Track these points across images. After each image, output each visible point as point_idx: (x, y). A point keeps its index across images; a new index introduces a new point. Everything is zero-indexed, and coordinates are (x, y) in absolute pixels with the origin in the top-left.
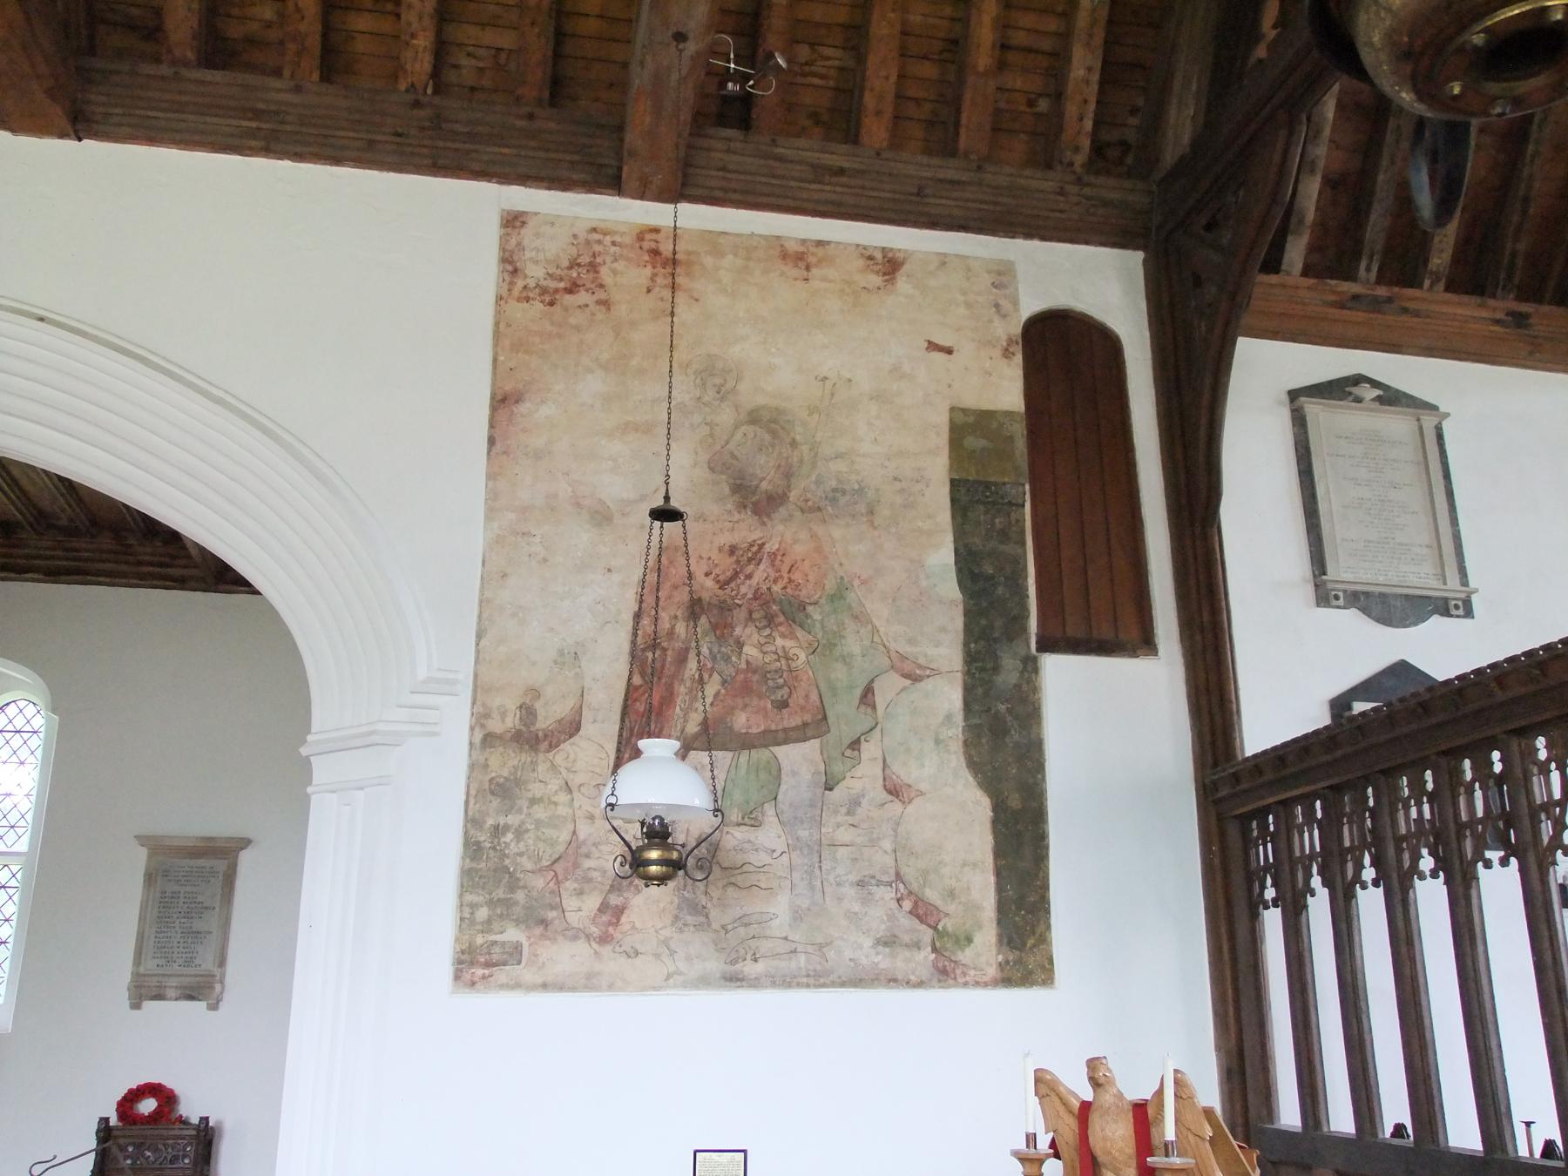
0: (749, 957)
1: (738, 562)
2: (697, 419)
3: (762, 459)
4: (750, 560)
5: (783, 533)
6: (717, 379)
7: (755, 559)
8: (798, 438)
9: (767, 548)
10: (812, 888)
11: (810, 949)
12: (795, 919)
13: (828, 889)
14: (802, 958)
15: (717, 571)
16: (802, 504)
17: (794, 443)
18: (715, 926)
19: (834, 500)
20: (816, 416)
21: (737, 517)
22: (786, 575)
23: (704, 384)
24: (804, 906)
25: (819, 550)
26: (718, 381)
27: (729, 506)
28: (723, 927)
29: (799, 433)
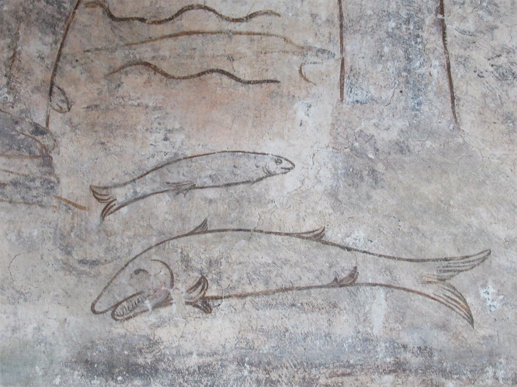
0: (180, 292)
10: (411, 82)
11: (407, 276)
12: (353, 176)
13: (469, 89)
14: (378, 307)
18: (70, 187)
24: (385, 137)
28: (97, 193)
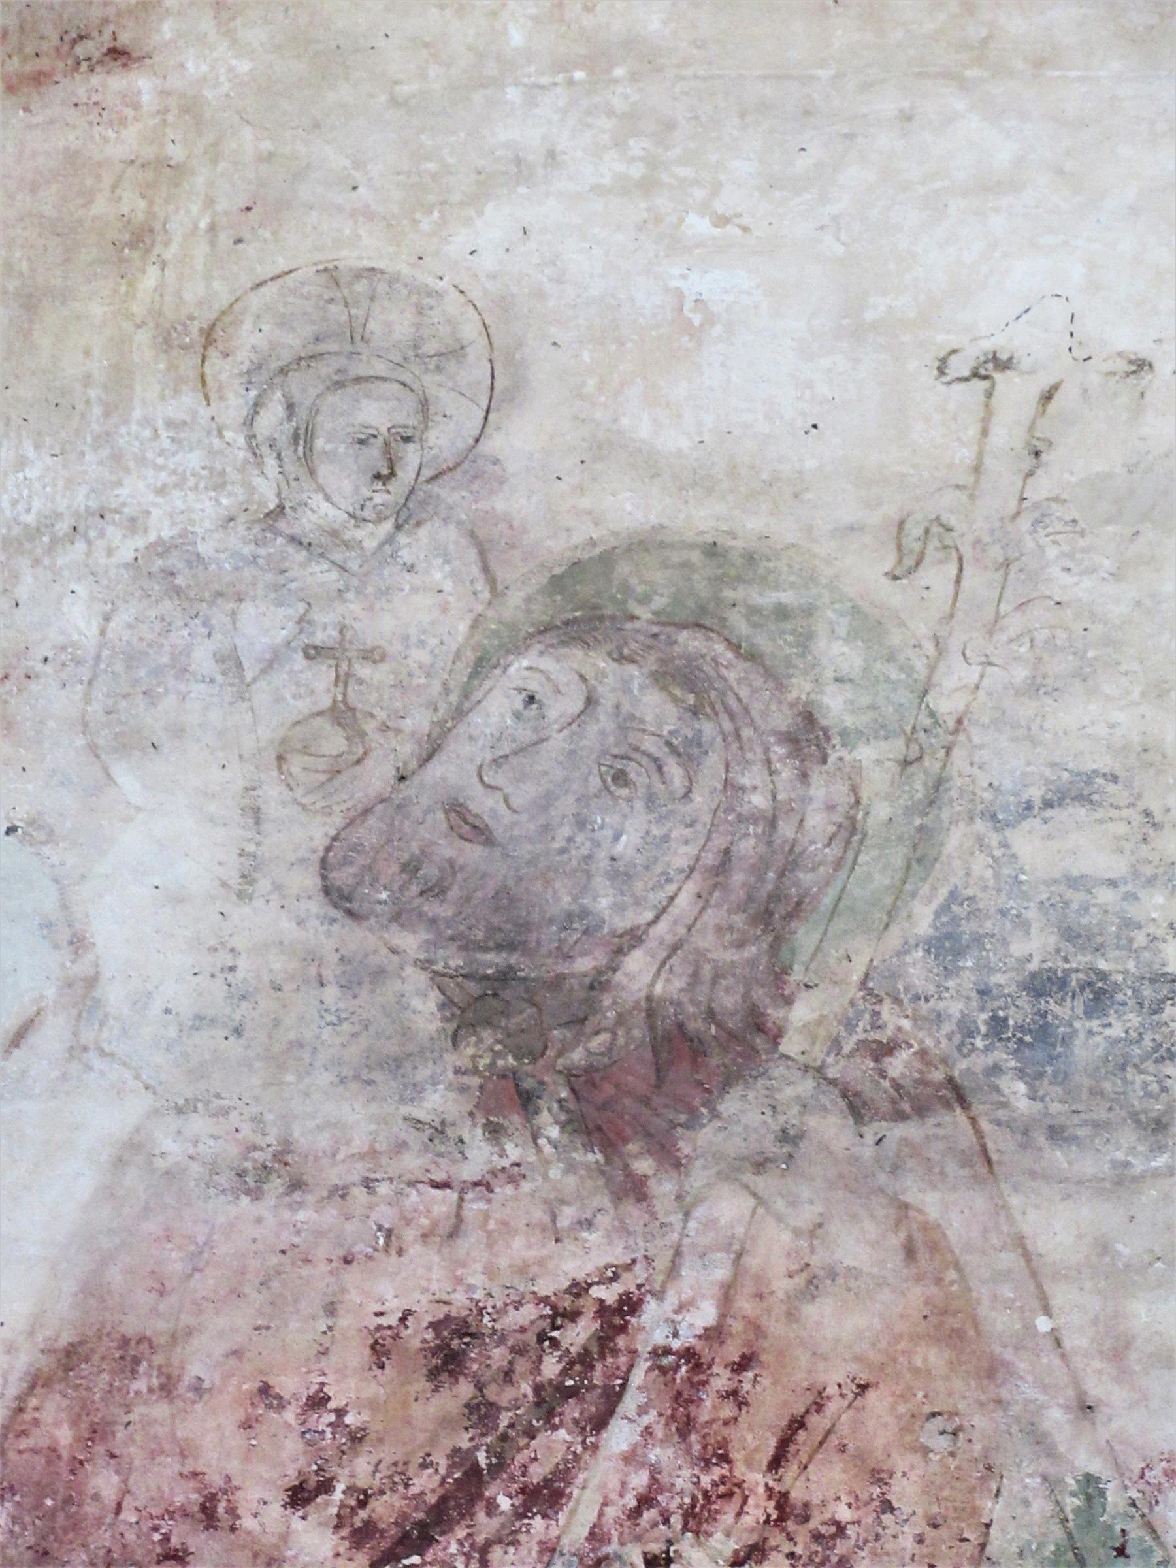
1: (481, 1413)
2: (262, 626)
3: (627, 831)
4: (549, 1402)
5: (734, 1234)
6: (367, 400)
7: (584, 1395)
8: (835, 706)
9: (653, 1326)
15: (361, 1469)
16: (857, 1071)
17: (808, 737)
19: (1039, 1043)
20: (937, 577)
21: (480, 1156)
22: (757, 1479)
23: (303, 437)
25: (951, 1325)
26: (376, 413)
27: (438, 1101)
29: (836, 677)
